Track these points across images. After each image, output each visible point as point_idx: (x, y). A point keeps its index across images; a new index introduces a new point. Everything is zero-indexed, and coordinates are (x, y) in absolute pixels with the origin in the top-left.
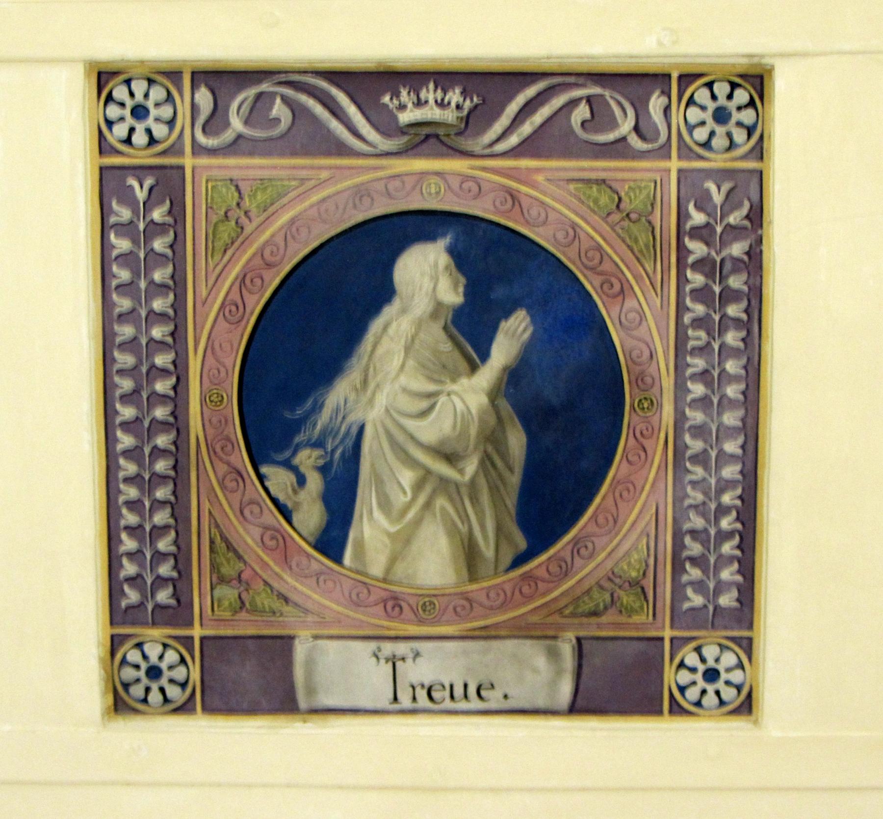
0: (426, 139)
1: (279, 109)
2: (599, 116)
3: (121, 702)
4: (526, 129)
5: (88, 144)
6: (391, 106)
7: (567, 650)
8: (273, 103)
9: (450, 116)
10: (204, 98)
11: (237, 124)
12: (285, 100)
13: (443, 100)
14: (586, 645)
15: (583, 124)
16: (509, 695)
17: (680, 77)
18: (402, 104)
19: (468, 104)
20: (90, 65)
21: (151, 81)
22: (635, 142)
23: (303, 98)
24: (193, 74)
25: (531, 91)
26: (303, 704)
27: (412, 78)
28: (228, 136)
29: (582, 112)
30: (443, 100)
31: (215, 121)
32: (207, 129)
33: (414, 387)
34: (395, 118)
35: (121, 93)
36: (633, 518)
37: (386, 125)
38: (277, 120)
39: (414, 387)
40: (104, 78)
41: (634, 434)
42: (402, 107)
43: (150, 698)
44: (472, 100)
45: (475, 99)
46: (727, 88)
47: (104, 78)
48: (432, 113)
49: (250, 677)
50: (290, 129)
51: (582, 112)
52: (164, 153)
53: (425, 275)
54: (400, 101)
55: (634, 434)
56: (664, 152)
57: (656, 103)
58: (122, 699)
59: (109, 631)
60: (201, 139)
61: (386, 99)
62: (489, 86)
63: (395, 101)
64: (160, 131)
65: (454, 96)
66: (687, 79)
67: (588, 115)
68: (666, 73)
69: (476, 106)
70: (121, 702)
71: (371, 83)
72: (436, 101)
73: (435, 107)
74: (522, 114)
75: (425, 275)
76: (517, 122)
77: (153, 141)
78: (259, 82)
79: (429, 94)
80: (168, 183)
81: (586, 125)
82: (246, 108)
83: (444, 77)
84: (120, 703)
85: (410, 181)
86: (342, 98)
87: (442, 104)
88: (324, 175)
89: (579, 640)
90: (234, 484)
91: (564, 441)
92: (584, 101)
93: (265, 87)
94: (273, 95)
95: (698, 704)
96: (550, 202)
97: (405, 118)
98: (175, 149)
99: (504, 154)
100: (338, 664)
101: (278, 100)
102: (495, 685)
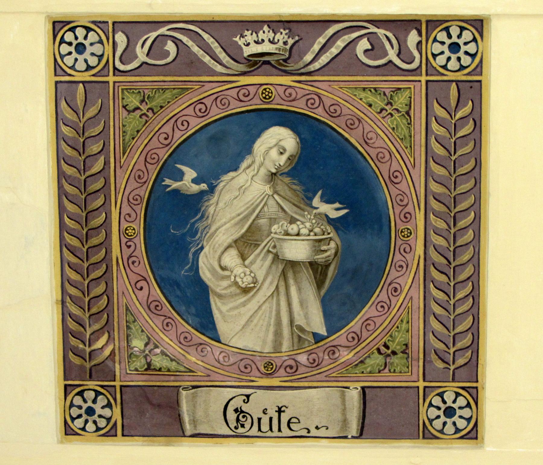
1: (170, 47)
2: (376, 50)
7: (354, 395)
10: (121, 39)
11: (141, 54)
12: (176, 41)
13: (274, 38)
14: (367, 391)
15: (366, 51)
17: (114, 23)
19: (291, 42)
20: (48, 17)
21: (88, 29)
23: (185, 39)
24: (428, 22)
25: (331, 31)
26: (189, 428)
28: (135, 64)
29: (364, 44)
30: (274, 38)
36: (404, 294)
38: (168, 53)
40: (59, 26)
48: (266, 47)
49: (155, 412)
57: (413, 38)
59: (63, 383)
60: (118, 64)
61: (237, 39)
72: (269, 40)
75: (277, 144)
76: (323, 51)
79: (266, 34)
83: (276, 24)
89: (363, 388)
90: (369, 136)
93: (163, 30)
95: (441, 431)
96: (345, 102)
97: (247, 51)
100: (205, 406)
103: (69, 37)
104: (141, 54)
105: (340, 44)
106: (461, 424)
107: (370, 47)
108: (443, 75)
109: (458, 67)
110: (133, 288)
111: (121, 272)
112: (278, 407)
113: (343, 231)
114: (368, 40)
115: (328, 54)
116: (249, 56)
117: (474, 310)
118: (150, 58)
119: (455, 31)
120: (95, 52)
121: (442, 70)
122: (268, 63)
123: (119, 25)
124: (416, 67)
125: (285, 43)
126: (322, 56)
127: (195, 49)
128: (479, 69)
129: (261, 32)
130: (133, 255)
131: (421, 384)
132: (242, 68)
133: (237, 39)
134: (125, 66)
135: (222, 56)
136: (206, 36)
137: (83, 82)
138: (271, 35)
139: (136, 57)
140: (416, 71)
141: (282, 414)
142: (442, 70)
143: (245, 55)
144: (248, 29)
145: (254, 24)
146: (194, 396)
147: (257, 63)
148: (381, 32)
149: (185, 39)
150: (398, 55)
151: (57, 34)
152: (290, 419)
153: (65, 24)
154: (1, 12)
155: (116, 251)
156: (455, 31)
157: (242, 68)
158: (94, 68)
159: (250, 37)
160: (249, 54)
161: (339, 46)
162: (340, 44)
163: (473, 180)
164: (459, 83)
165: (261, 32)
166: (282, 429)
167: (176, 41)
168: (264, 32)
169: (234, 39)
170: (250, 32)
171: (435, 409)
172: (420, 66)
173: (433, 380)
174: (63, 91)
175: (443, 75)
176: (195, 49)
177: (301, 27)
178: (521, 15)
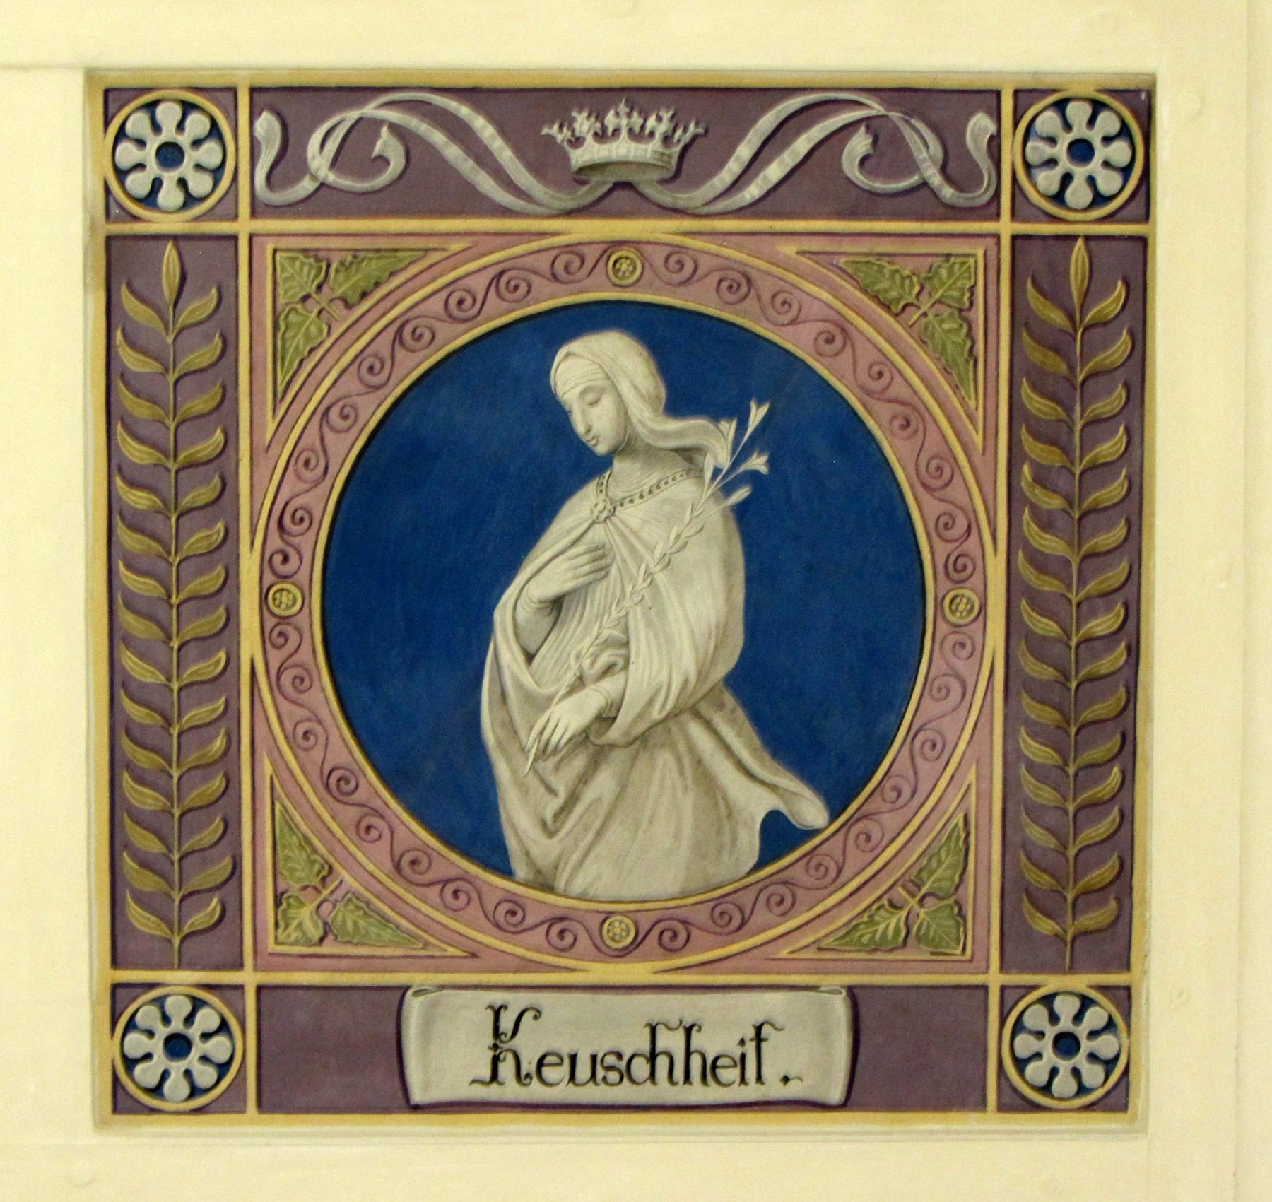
0: (619, 191)
1: (386, 144)
2: (888, 151)
3: (126, 1099)
6: (559, 138)
8: (377, 136)
9: (647, 151)
10: (267, 124)
11: (318, 157)
12: (394, 128)
13: (643, 127)
15: (864, 160)
18: (577, 134)
20: (91, 76)
28: (306, 186)
29: (860, 144)
30: (643, 127)
31: (288, 161)
33: (634, 589)
34: (567, 159)
35: (138, 124)
37: (546, 160)
38: (383, 161)
39: (634, 589)
40: (116, 99)
41: (449, 296)
42: (577, 142)
46: (1087, 110)
47: (116, 99)
48: (622, 149)
49: (332, 1058)
50: (401, 176)
51: (860, 144)
52: (208, 215)
54: (573, 131)
55: (449, 296)
56: (990, 210)
62: (712, 110)
64: (200, 184)
65: (659, 124)
66: (1024, 97)
68: (994, 88)
69: (695, 137)
70: (1115, 1096)
71: (532, 108)
72: (630, 131)
74: (766, 149)
78: (362, 103)
80: (211, 256)
82: (332, 145)
83: (641, 96)
85: (591, 255)
86: (483, 128)
87: (638, 135)
88: (456, 246)
91: (822, 657)
92: (862, 129)
93: (370, 110)
94: (379, 123)
99: (740, 212)
101: (385, 131)
105: (802, 144)
106: (1093, 1074)
109: (129, 128)
110: (292, 739)
111: (262, 701)
113: (679, 760)
114: (868, 128)
117: (1129, 592)
123: (268, 96)
124: (402, 162)
125: (667, 139)
127: (453, 152)
131: (995, 979)
133: (554, 130)
135: (523, 177)
137: (175, 238)
138: (637, 120)
141: (764, 1045)
145: (598, 97)
146: (434, 1004)
150: (943, 170)
151: (114, 116)
153: (1017, 191)
154: (8, 67)
155: (250, 645)
158: (202, 199)
159: (583, 124)
162: (802, 144)
163: (1118, 737)
165: (612, 113)
168: (617, 114)
171: (1032, 1038)
172: (997, 195)
173: (1026, 976)
174: (121, 260)
176: (453, 152)
178: (617, 798)
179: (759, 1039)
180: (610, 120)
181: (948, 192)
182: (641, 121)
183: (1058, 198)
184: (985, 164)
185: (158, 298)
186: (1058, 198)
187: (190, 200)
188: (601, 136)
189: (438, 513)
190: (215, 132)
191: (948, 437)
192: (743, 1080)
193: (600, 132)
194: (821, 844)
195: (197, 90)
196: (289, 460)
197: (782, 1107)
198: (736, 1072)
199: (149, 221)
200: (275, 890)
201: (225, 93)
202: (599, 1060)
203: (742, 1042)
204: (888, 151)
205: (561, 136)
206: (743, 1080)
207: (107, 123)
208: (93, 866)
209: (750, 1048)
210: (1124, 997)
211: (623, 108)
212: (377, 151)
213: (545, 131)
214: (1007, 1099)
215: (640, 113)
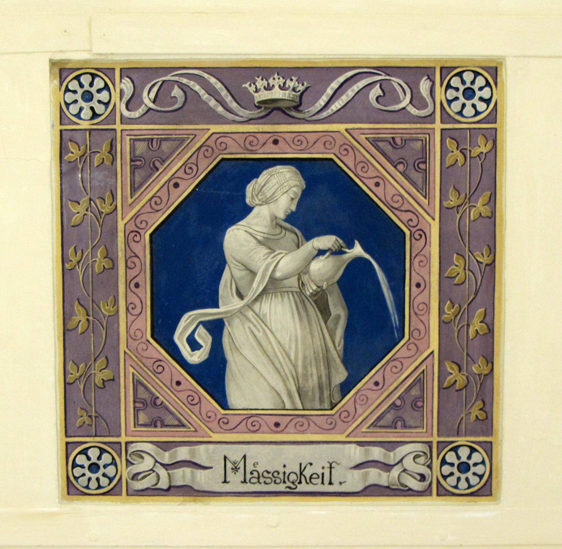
1: (177, 92)
2: (388, 94)
4: (344, 99)
5: (60, 471)
10: (127, 86)
11: (147, 100)
12: (182, 87)
15: (377, 99)
16: (287, 466)
19: (301, 88)
20: (53, 63)
22: (413, 111)
23: (192, 84)
25: (341, 79)
27: (265, 71)
29: (376, 91)
32: (129, 108)
37: (243, 99)
42: (257, 91)
43: (101, 484)
44: (303, 85)
45: (305, 83)
47: (63, 71)
48: (277, 94)
53: (277, 192)
58: (71, 482)
59: (59, 127)
60: (126, 113)
63: (253, 86)
64: (100, 109)
66: (445, 70)
67: (380, 93)
69: (307, 89)
70: (72, 489)
72: (280, 86)
73: (279, 90)
75: (277, 192)
77: (95, 115)
81: (380, 99)
83: (286, 71)
84: (70, 485)
87: (283, 88)
97: (265, 95)
98: (111, 119)
102: (311, 462)
103: (480, 82)
104: (147, 100)
105: (350, 93)
107: (382, 94)
108: (77, 124)
112: (329, 462)
115: (340, 101)
116: (259, 102)
118: (156, 105)
119: (86, 80)
120: (101, 100)
121: (458, 118)
122: (279, 109)
123: (126, 72)
126: (334, 102)
128: (493, 117)
129: (272, 78)
130: (136, 317)
132: (255, 113)
133: (247, 85)
134: (130, 113)
135: (234, 105)
136: (213, 80)
139: (142, 102)
140: (430, 118)
141: (333, 470)
142: (75, 119)
143: (256, 101)
144: (280, 73)
147: (272, 110)
148: (395, 81)
149: (192, 84)
152: (312, 475)
156: (86, 80)
157: (255, 113)
159: (260, 83)
160: (260, 100)
161: (226, 95)
162: (350, 93)
164: (472, 131)
165: (272, 78)
166: (333, 481)
167: (182, 87)
168: (274, 79)
169: (244, 86)
170: (261, 78)
172: (434, 112)
175: (77, 124)
177: (314, 75)
179: (331, 468)
180: (271, 81)
181: (413, 111)
182: (266, 82)
183: (460, 113)
184: (429, 100)
185: (81, 156)
186: (460, 113)
187: (95, 115)
188: (269, 88)
189: (185, 264)
190: (106, 87)
191: (421, 213)
192: (323, 483)
193: (266, 86)
194: (264, 415)
195: (97, 69)
196: (142, 210)
197: (267, 495)
198: (320, 480)
199: (79, 124)
200: (400, 173)
201: (109, 71)
202: (286, 475)
203: (323, 468)
204: (388, 94)
205: (252, 89)
206: (323, 483)
207: (61, 84)
208: (57, 381)
209: (327, 472)
210: (489, 448)
211: (276, 76)
212: (172, 95)
213: (244, 86)
214: (442, 491)
215: (283, 78)
